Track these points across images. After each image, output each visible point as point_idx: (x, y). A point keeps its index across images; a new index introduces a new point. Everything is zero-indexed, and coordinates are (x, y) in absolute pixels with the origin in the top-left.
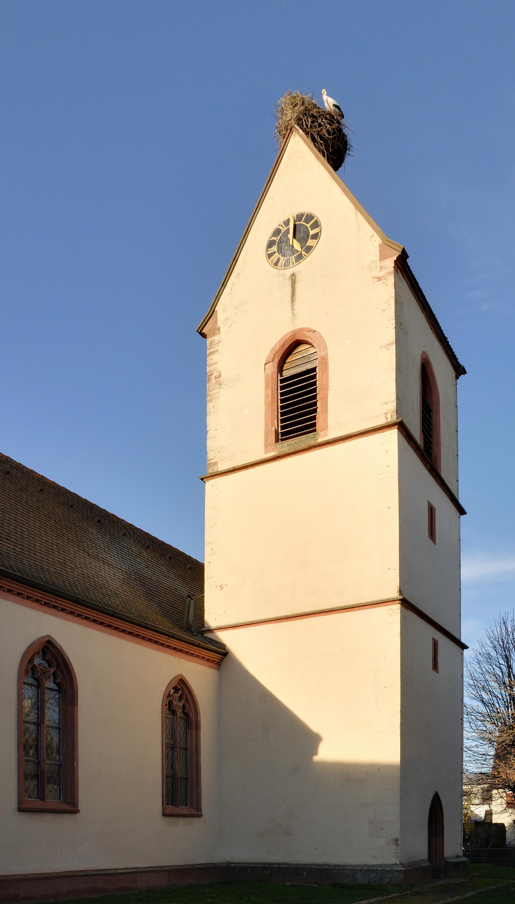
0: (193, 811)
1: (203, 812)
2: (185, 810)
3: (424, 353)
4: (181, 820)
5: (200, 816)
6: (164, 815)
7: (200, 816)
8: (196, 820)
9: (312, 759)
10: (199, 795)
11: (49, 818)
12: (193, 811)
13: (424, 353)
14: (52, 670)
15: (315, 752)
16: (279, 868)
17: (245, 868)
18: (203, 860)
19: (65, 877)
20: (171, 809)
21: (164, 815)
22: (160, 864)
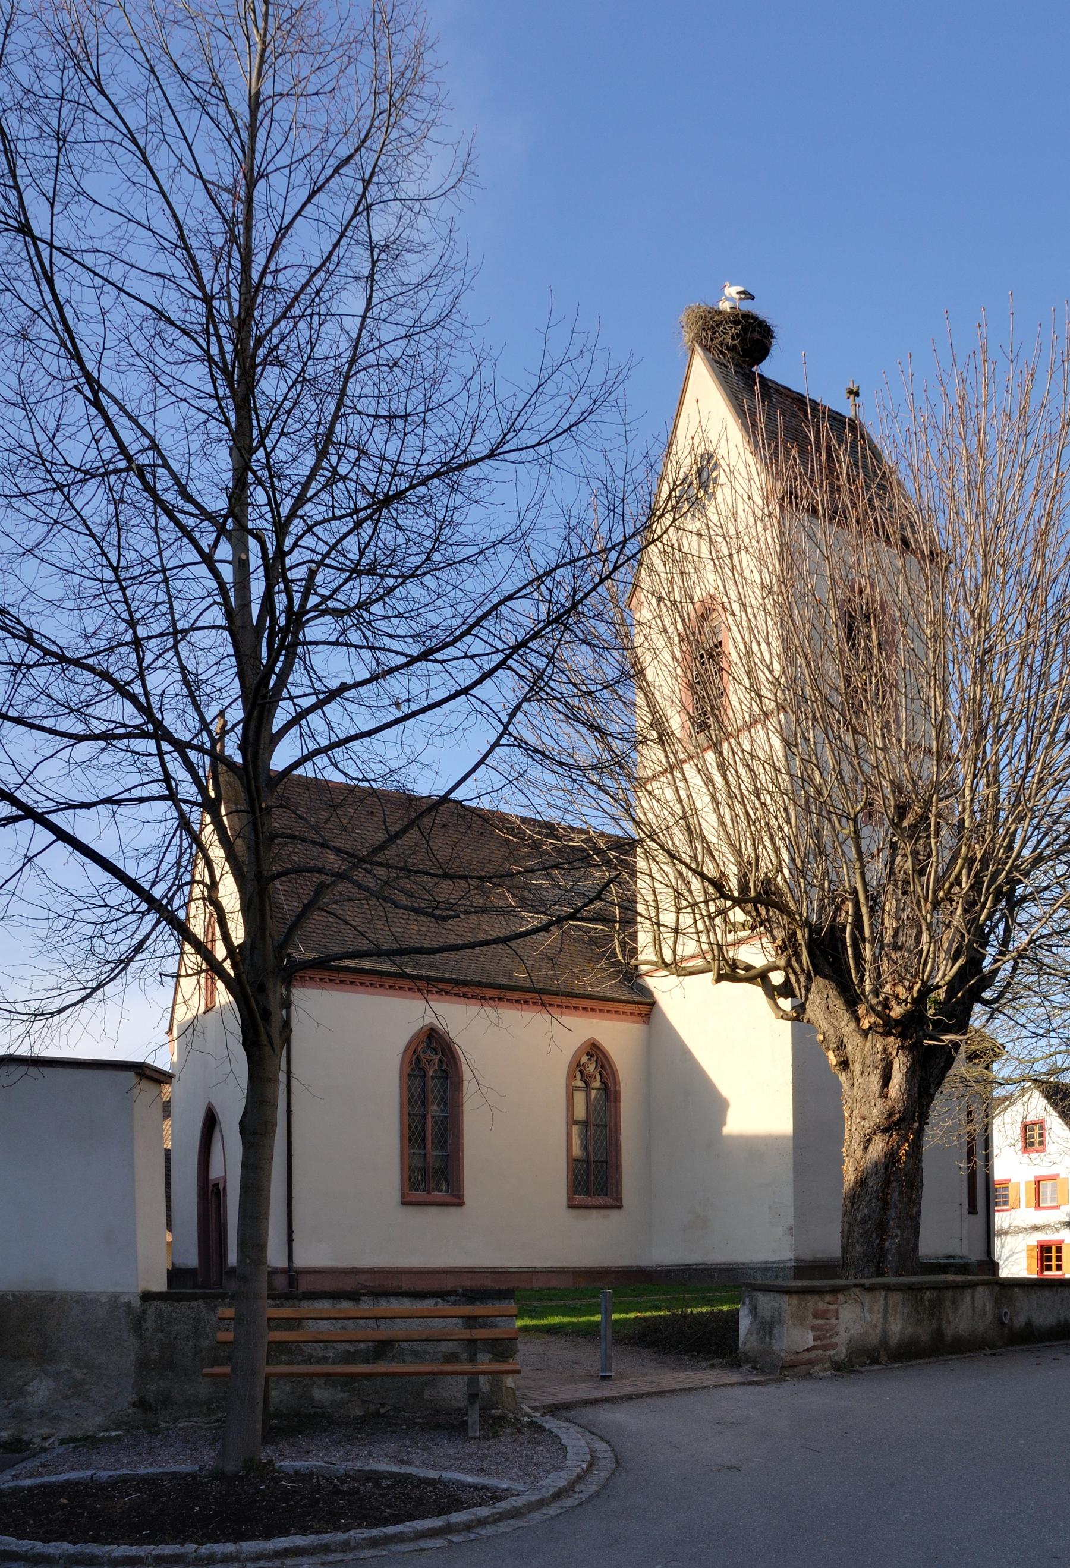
0: (611, 1202)
1: (624, 1203)
2: (600, 1200)
3: (209, 1103)
4: (594, 1213)
5: (620, 1207)
6: (571, 1207)
7: (620, 1207)
8: (614, 1214)
9: (721, 1130)
10: (618, 1182)
11: (433, 1211)
12: (611, 1202)
13: (209, 1103)
14: (437, 1058)
15: (723, 1123)
16: (696, 1270)
17: (670, 1271)
18: (626, 1262)
19: (451, 1272)
20: (580, 1199)
21: (571, 1207)
22: (565, 1264)
